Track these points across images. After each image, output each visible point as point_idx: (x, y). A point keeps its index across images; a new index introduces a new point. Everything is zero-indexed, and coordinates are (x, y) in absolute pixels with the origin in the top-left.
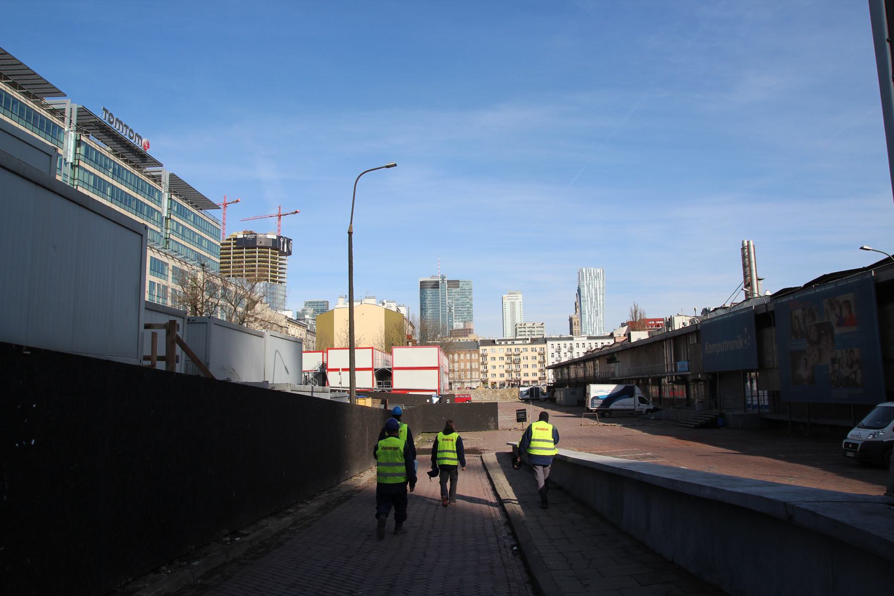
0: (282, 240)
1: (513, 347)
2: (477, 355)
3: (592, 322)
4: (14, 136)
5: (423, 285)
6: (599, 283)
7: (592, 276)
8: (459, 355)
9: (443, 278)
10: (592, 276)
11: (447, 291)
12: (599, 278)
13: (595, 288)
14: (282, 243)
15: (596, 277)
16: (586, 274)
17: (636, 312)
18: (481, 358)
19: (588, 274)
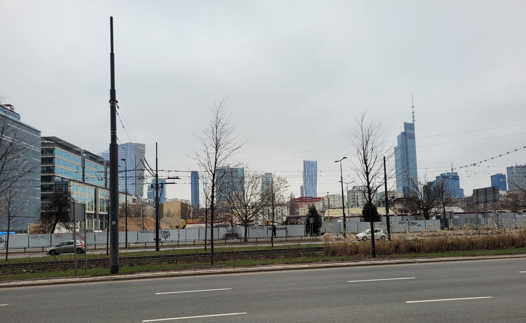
3: (313, 193)
4: (95, 238)
7: (310, 165)
10: (310, 165)
12: (314, 165)
15: (312, 165)
16: (307, 163)
17: (292, 195)
19: (308, 164)
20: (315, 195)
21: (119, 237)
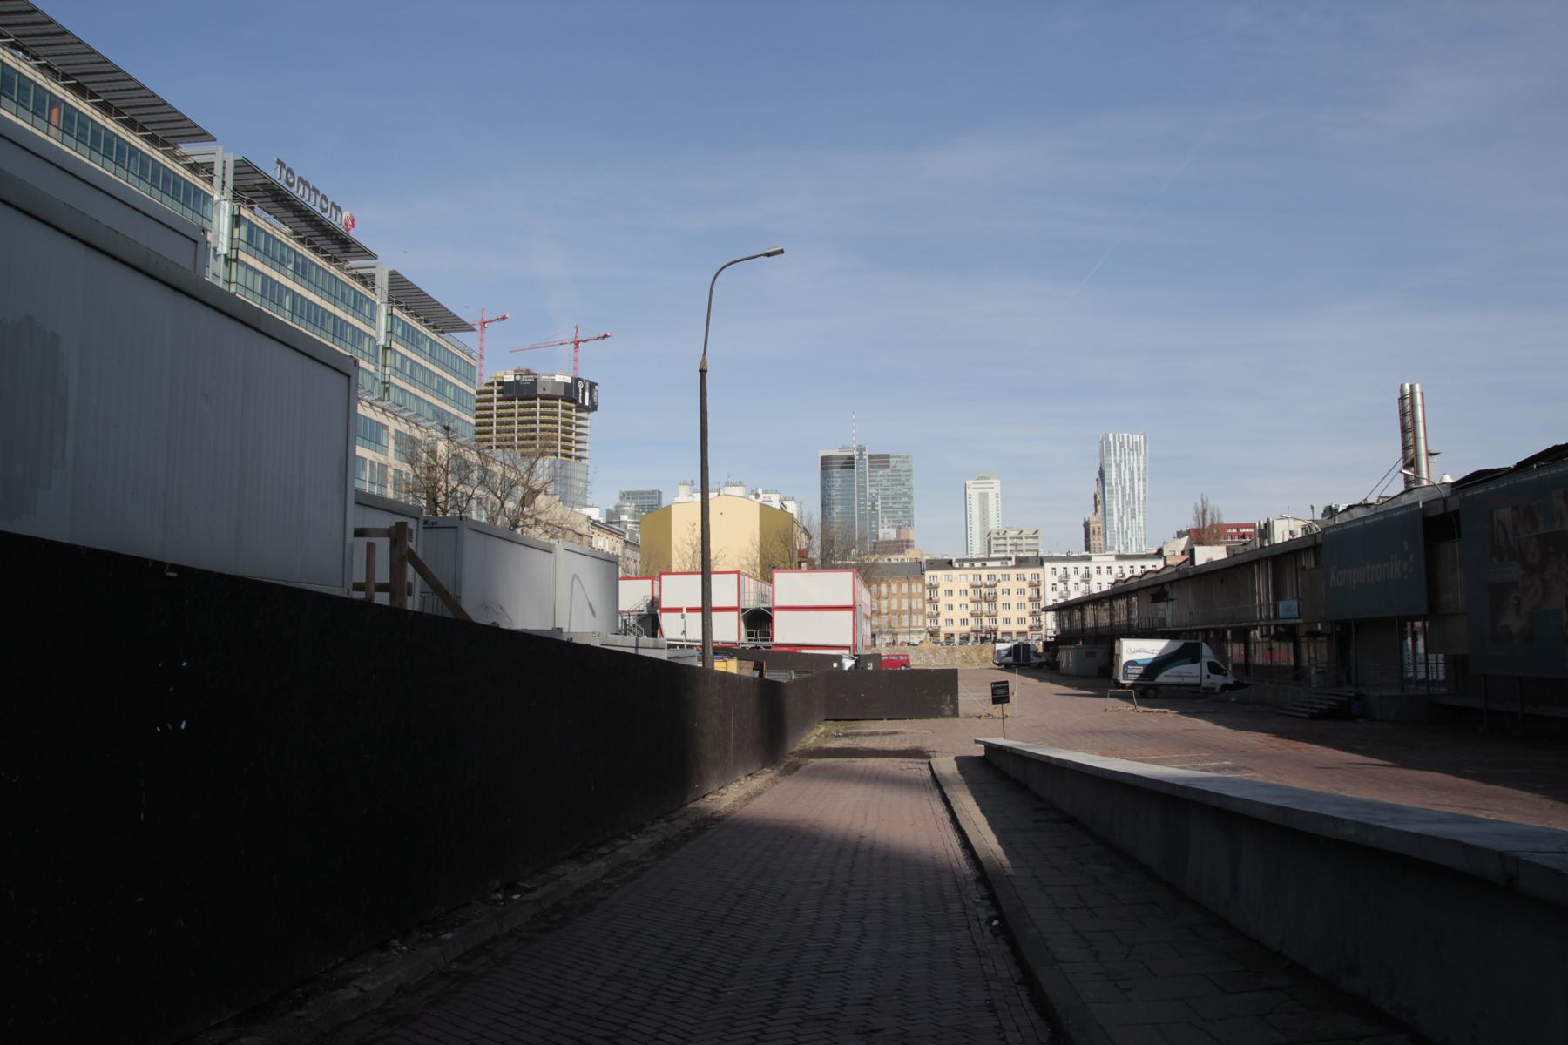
0: (580, 385)
1: (984, 573)
2: (920, 586)
5: (826, 463)
6: (1138, 460)
7: (1126, 447)
8: (889, 586)
9: (861, 450)
10: (1126, 447)
11: (868, 474)
12: (1137, 450)
13: (1130, 468)
14: (580, 390)
15: (1132, 450)
18: (927, 591)
19: (1118, 444)
20: (1127, 548)
21: (1318, 747)
